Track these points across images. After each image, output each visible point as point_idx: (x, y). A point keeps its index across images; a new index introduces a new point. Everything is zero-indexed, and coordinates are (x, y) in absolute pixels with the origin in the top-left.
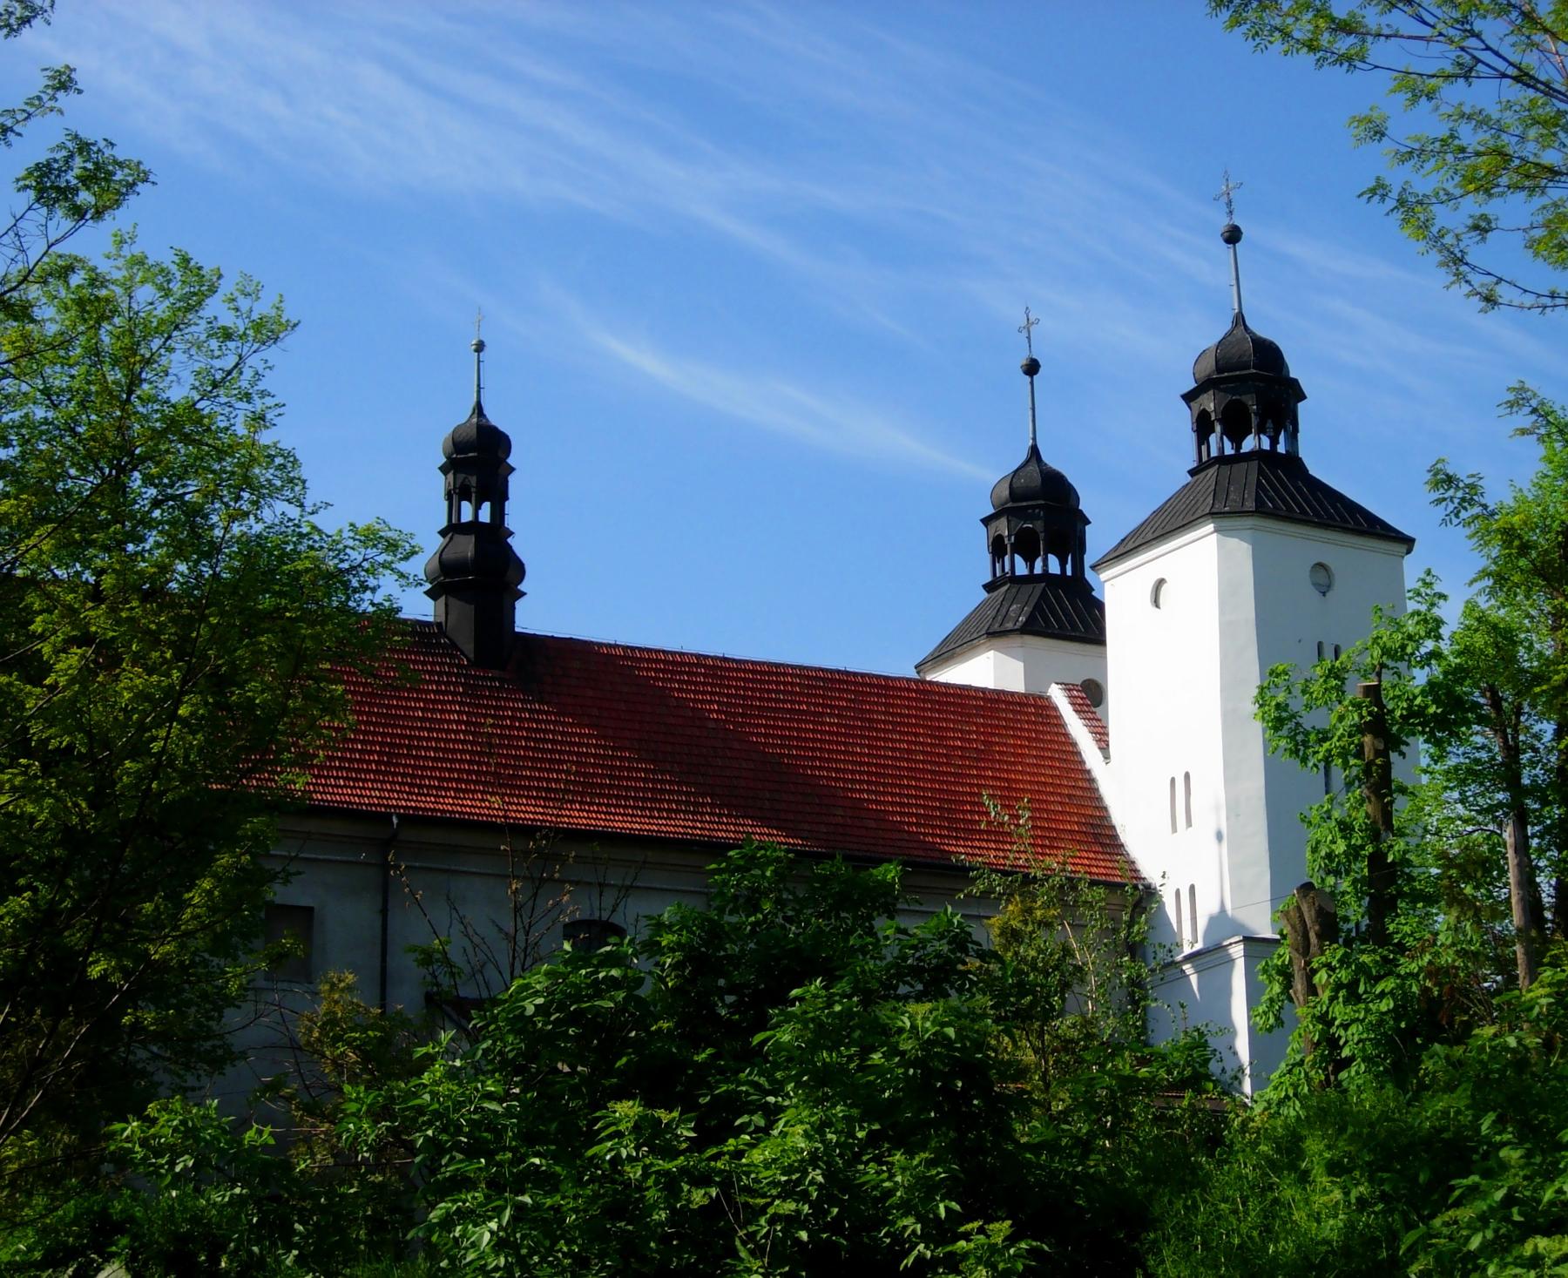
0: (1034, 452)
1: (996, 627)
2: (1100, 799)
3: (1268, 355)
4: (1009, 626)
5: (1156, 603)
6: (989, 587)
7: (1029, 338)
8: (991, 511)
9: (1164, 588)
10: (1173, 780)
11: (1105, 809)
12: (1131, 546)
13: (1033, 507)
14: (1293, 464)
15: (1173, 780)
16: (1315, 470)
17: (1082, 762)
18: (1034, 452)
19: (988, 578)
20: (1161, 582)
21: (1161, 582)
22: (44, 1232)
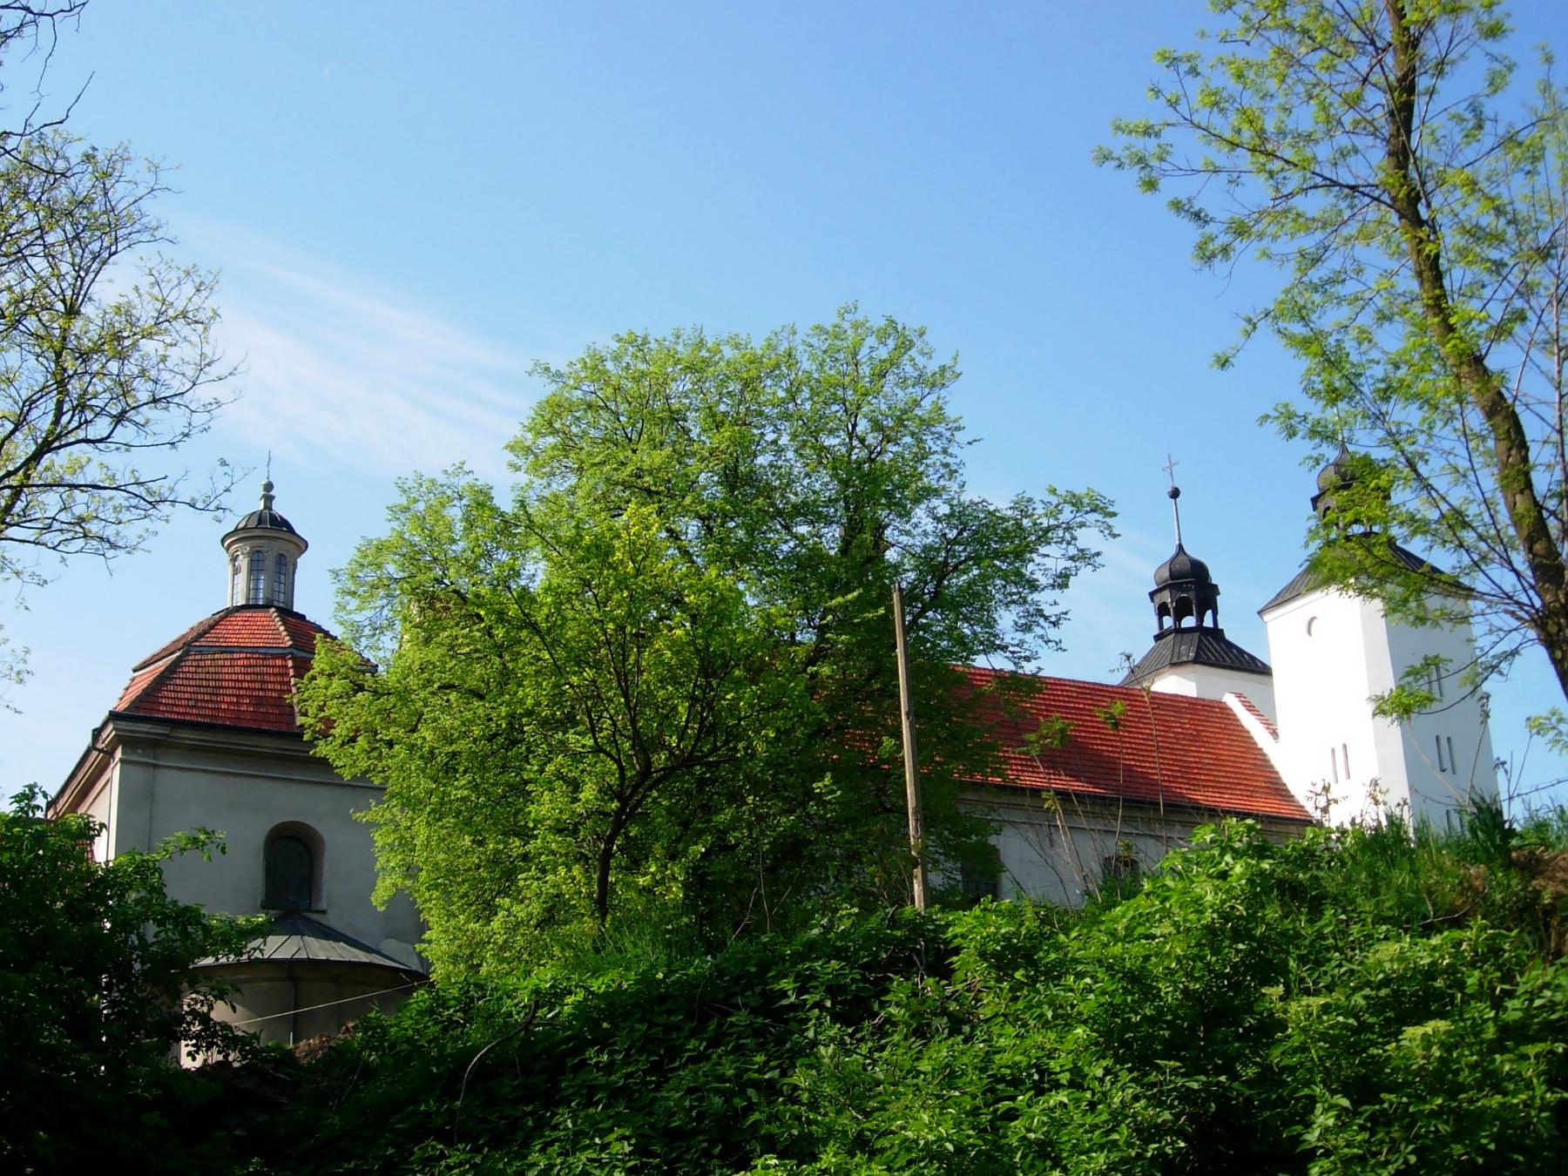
0: (1180, 547)
1: (1175, 660)
2: (1272, 767)
3: (1198, 572)
4: (1184, 659)
5: (1309, 632)
6: (1158, 638)
7: (1171, 474)
8: (1155, 587)
9: (1315, 624)
10: (1333, 750)
11: (1277, 773)
12: (1287, 596)
13: (1187, 583)
14: (1216, 633)
15: (1333, 750)
16: (1228, 636)
17: (1255, 744)
18: (1180, 547)
19: (1157, 632)
20: (1313, 619)
21: (1313, 619)
22: (709, 821)
